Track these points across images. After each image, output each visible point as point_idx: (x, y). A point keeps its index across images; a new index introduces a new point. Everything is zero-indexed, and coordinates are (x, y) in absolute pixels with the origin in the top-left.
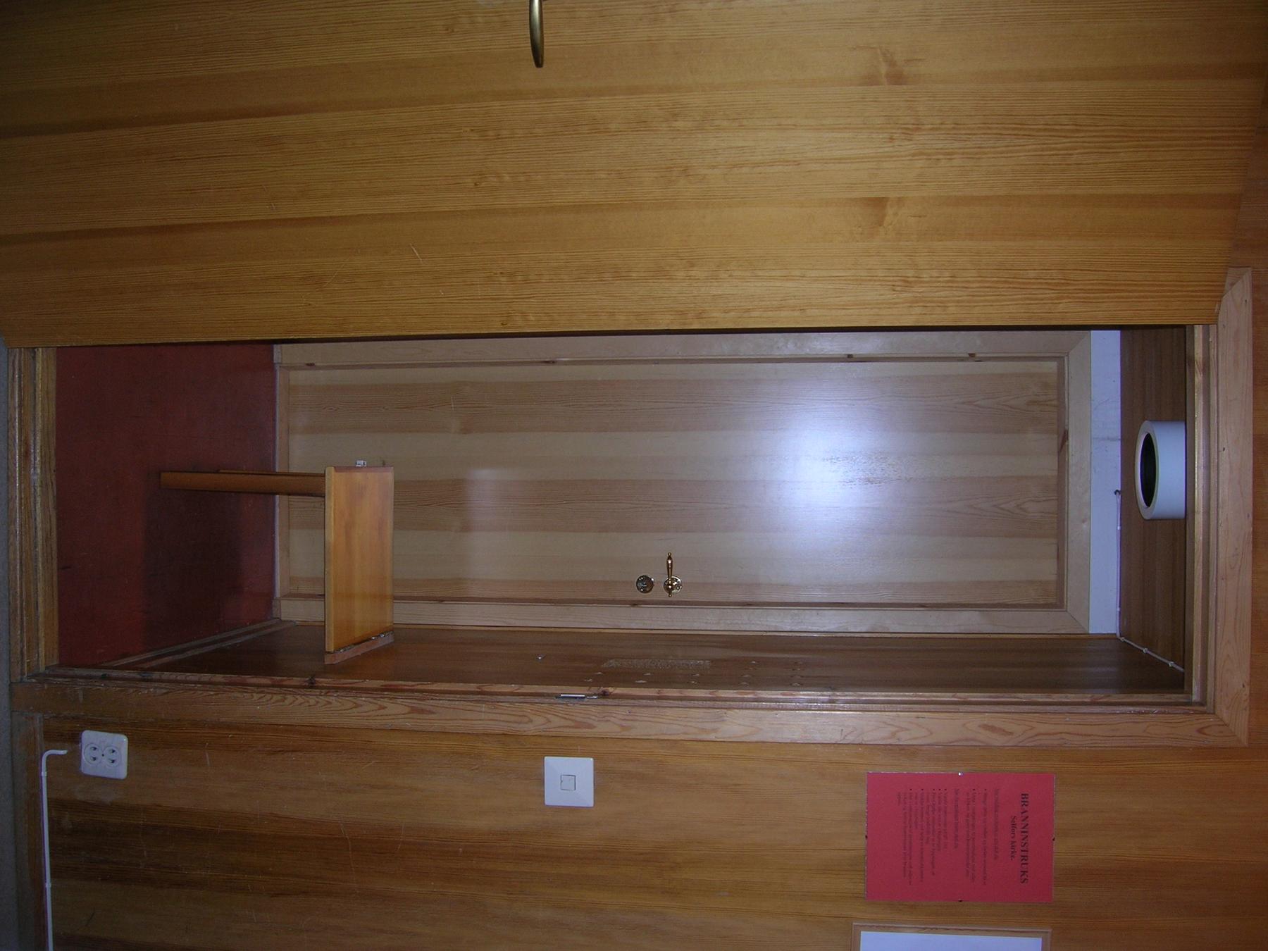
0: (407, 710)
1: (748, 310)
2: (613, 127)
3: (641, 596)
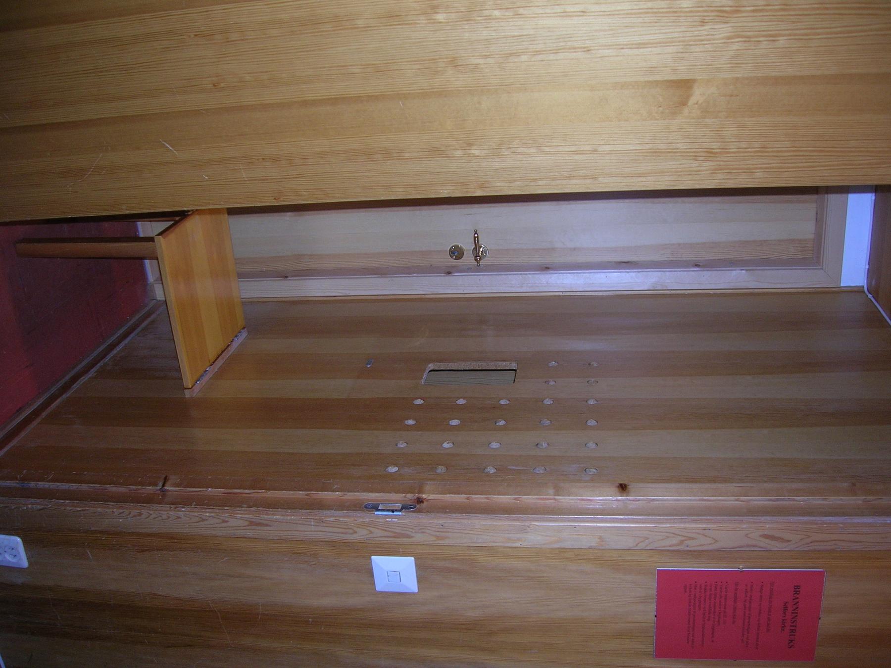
0: (246, 523)
1: (535, 180)
2: (360, 23)
3: (453, 262)
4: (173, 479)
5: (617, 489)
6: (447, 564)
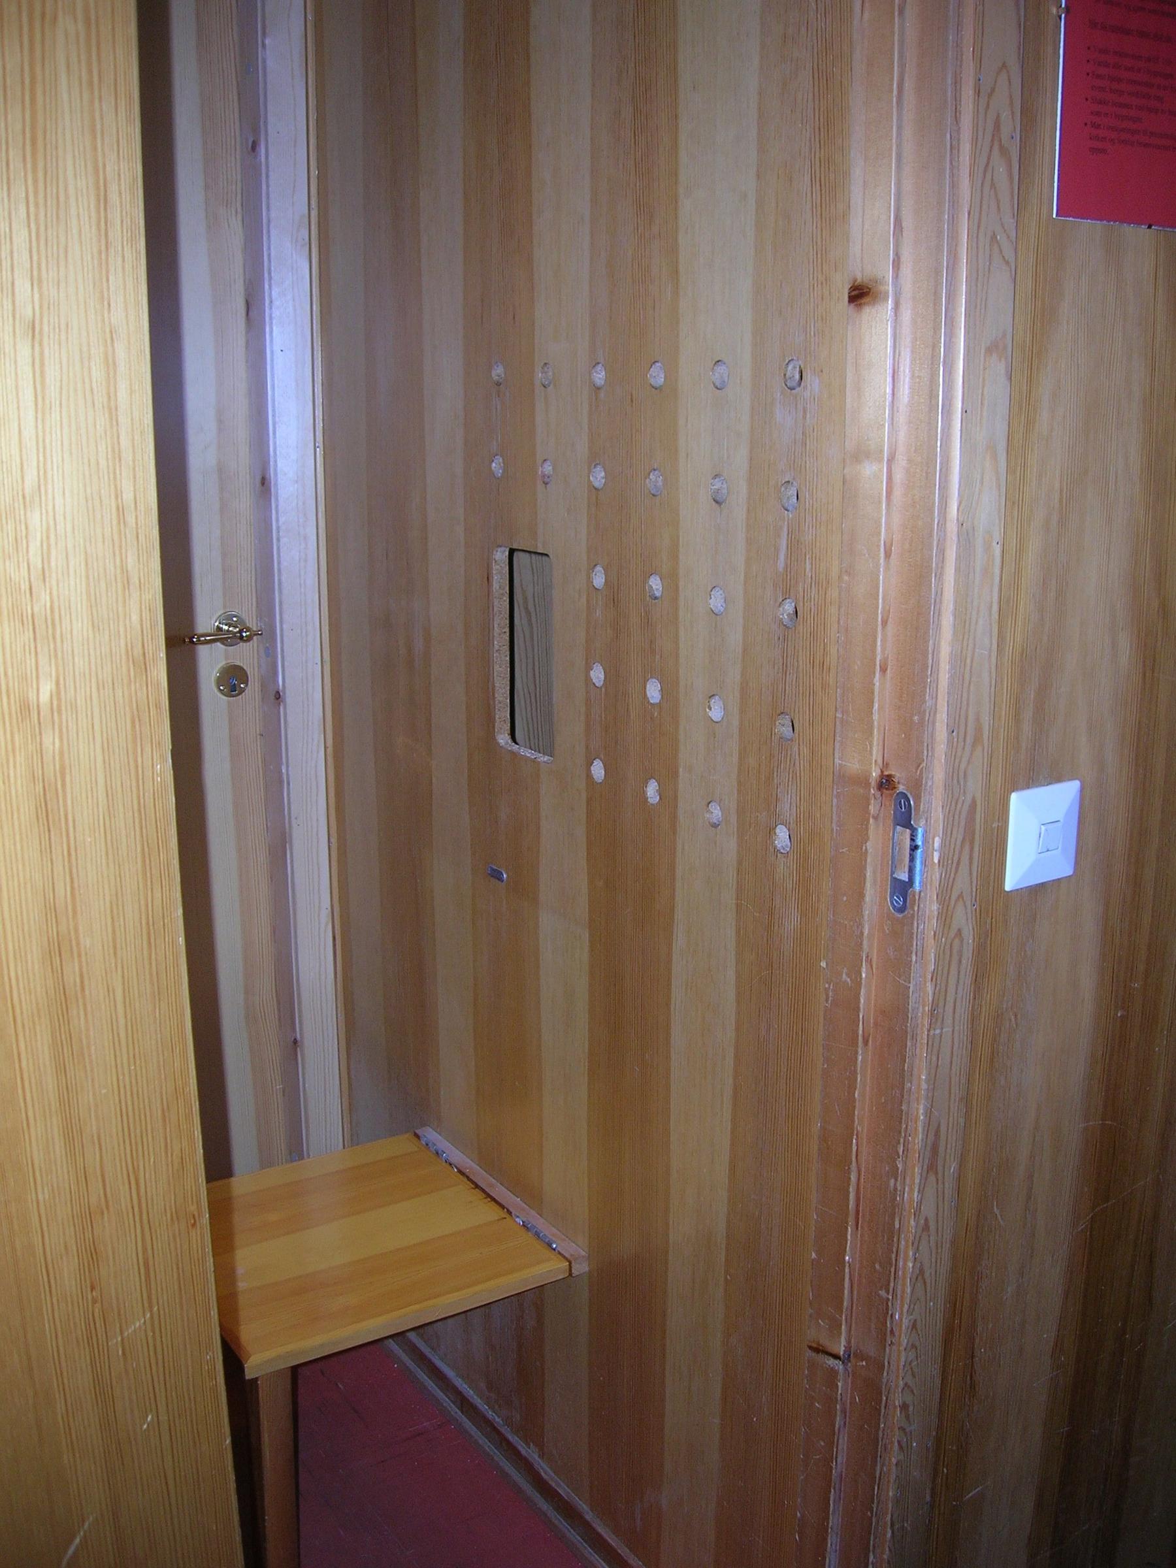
1: (121, 511)
3: (252, 690)
4: (817, 1332)
5: (867, 310)
6: (1028, 714)
